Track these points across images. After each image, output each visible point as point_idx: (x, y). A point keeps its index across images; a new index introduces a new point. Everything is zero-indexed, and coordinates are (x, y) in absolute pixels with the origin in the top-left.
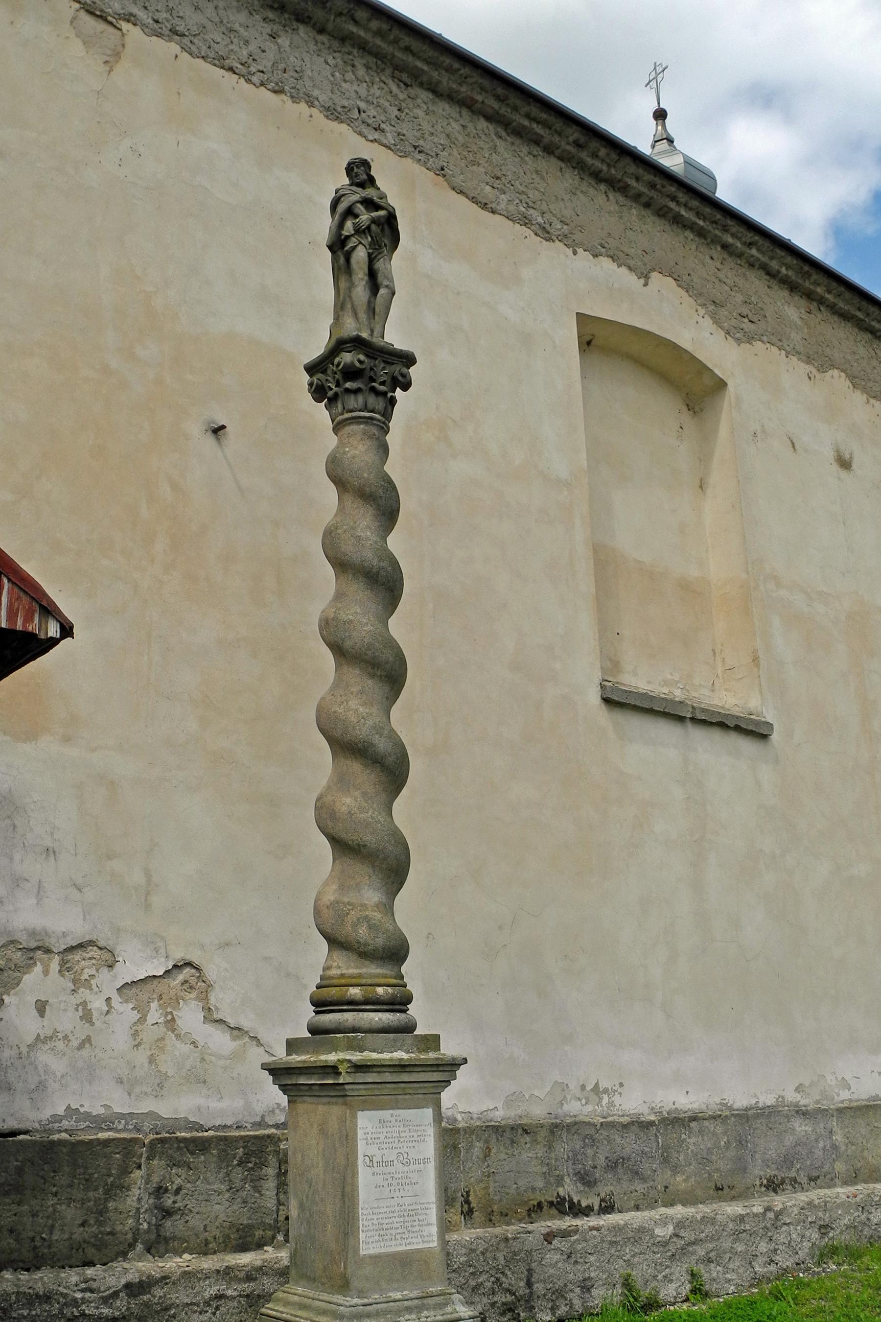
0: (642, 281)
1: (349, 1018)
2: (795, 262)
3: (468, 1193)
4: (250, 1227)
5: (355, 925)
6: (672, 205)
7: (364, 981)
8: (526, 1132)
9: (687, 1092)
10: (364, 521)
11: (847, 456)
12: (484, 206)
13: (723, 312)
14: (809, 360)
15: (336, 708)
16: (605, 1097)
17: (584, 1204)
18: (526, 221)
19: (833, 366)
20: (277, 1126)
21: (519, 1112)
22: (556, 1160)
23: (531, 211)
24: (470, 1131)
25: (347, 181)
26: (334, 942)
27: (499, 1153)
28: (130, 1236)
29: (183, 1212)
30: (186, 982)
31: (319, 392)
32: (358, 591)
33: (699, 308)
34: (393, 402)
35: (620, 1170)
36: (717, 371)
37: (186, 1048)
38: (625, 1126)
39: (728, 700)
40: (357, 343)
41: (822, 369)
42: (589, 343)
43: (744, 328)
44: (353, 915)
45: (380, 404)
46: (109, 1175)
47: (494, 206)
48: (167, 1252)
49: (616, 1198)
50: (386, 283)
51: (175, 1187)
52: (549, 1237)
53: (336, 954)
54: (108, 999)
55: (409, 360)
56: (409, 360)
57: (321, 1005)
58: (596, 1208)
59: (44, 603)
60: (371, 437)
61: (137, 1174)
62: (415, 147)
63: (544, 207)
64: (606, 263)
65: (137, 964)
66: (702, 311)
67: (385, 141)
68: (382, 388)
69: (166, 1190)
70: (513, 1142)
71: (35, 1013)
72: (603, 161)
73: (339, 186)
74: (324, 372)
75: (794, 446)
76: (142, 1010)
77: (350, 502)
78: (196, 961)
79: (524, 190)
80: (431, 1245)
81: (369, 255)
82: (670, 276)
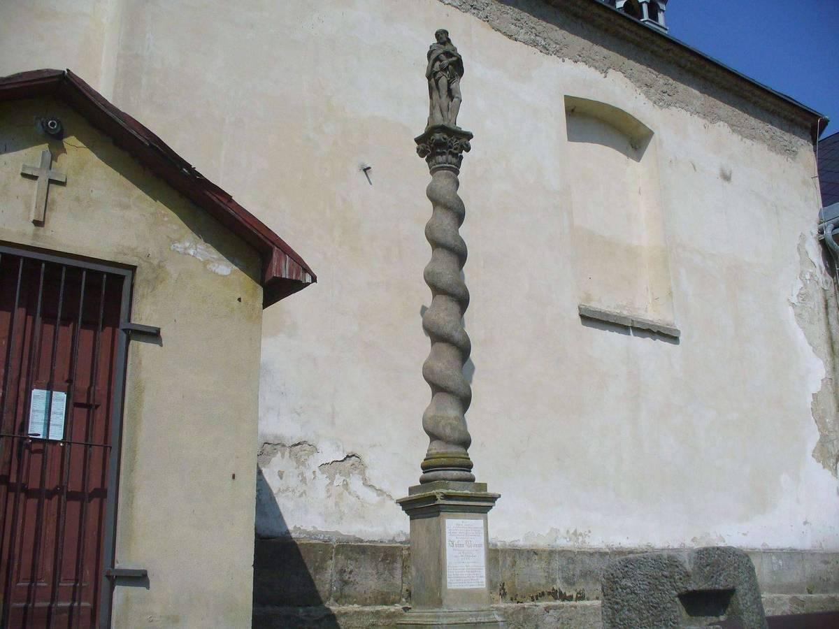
0: (603, 75)
1: (441, 474)
2: (695, 59)
3: (504, 584)
4: (388, 593)
5: (444, 427)
6: (621, 30)
7: (448, 456)
8: (535, 553)
9: (628, 538)
10: (447, 220)
11: (728, 173)
12: (510, 37)
13: (652, 90)
14: (705, 116)
15: (433, 317)
16: (580, 538)
17: (567, 595)
18: (535, 44)
19: (720, 119)
20: (401, 543)
21: (531, 543)
22: (552, 570)
23: (538, 38)
24: (504, 551)
25: (435, 41)
26: (434, 437)
27: (521, 563)
28: (327, 593)
29: (354, 583)
30: (353, 464)
31: (422, 153)
32: (444, 256)
33: (637, 89)
34: (461, 158)
35: (588, 578)
36: (647, 125)
37: (354, 499)
38: (592, 554)
39: (651, 314)
40: (443, 129)
41: (713, 122)
42: (573, 110)
43: (664, 99)
44: (443, 423)
45: (454, 160)
46: (317, 562)
47: (516, 36)
48: (346, 602)
49: (586, 592)
50: (457, 95)
51: (349, 570)
52: (547, 609)
53: (435, 443)
54: (314, 472)
55: (469, 136)
56: (469, 136)
57: (426, 468)
58: (575, 597)
59: (304, 267)
60: (450, 177)
61: (330, 562)
62: (472, 6)
63: (545, 35)
64: (582, 66)
65: (328, 453)
66: (639, 91)
67: (455, 4)
68: (455, 152)
69: (345, 571)
70: (528, 559)
71: (278, 477)
72: (579, 7)
73: (431, 44)
74: (425, 143)
75: (694, 168)
76: (332, 478)
77: (439, 211)
78: (359, 454)
79: (534, 26)
80: (483, 587)
81: (448, 81)
82: (620, 71)
